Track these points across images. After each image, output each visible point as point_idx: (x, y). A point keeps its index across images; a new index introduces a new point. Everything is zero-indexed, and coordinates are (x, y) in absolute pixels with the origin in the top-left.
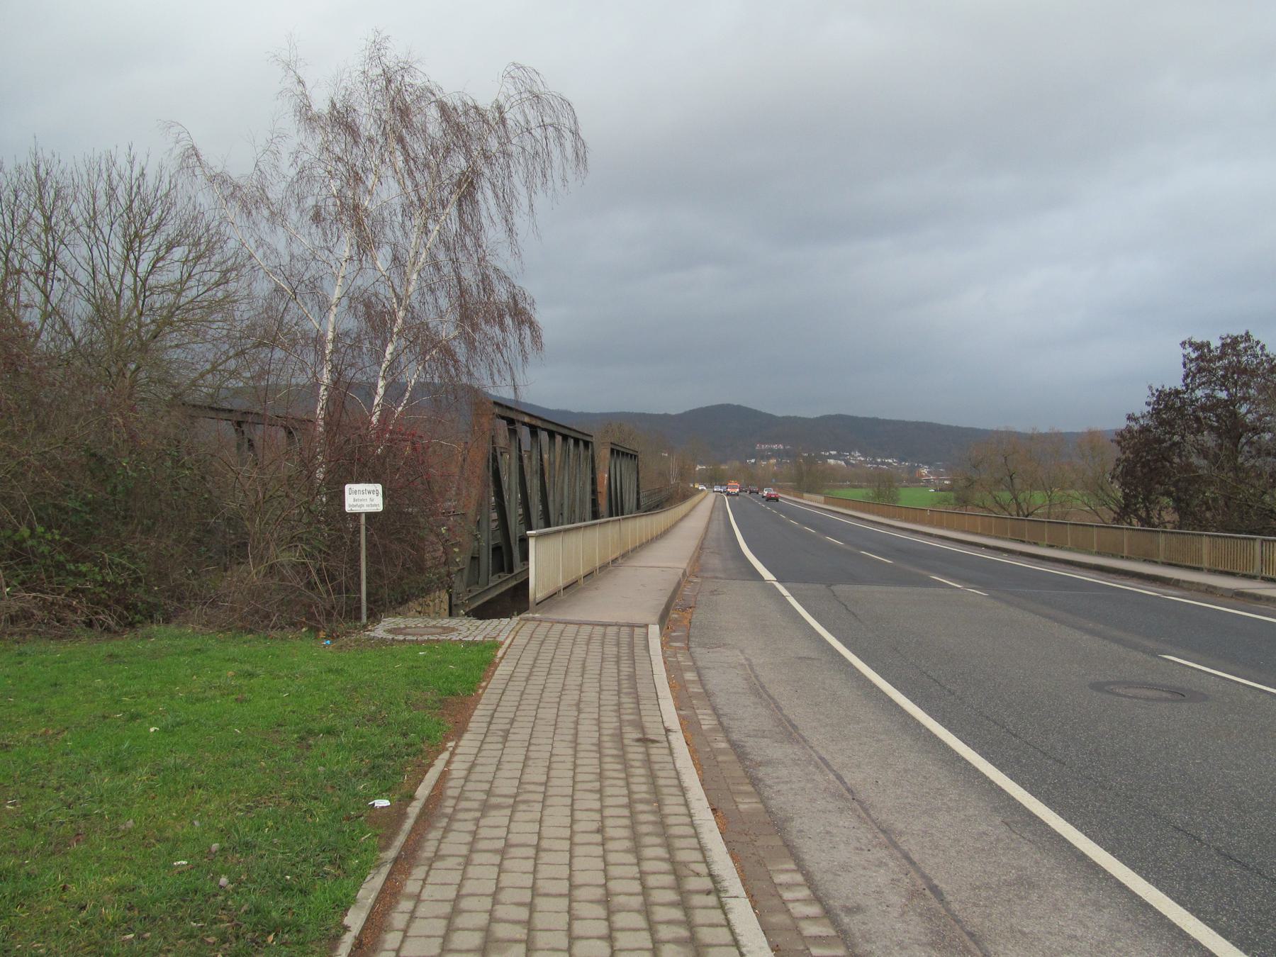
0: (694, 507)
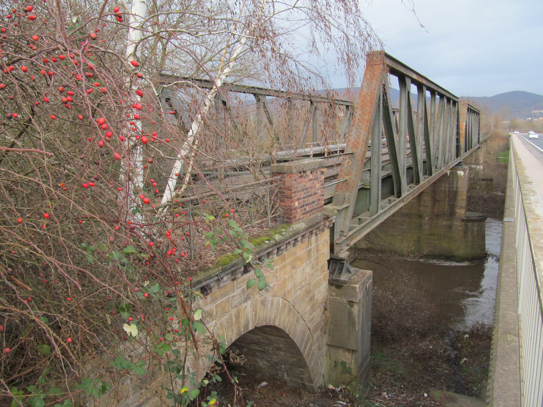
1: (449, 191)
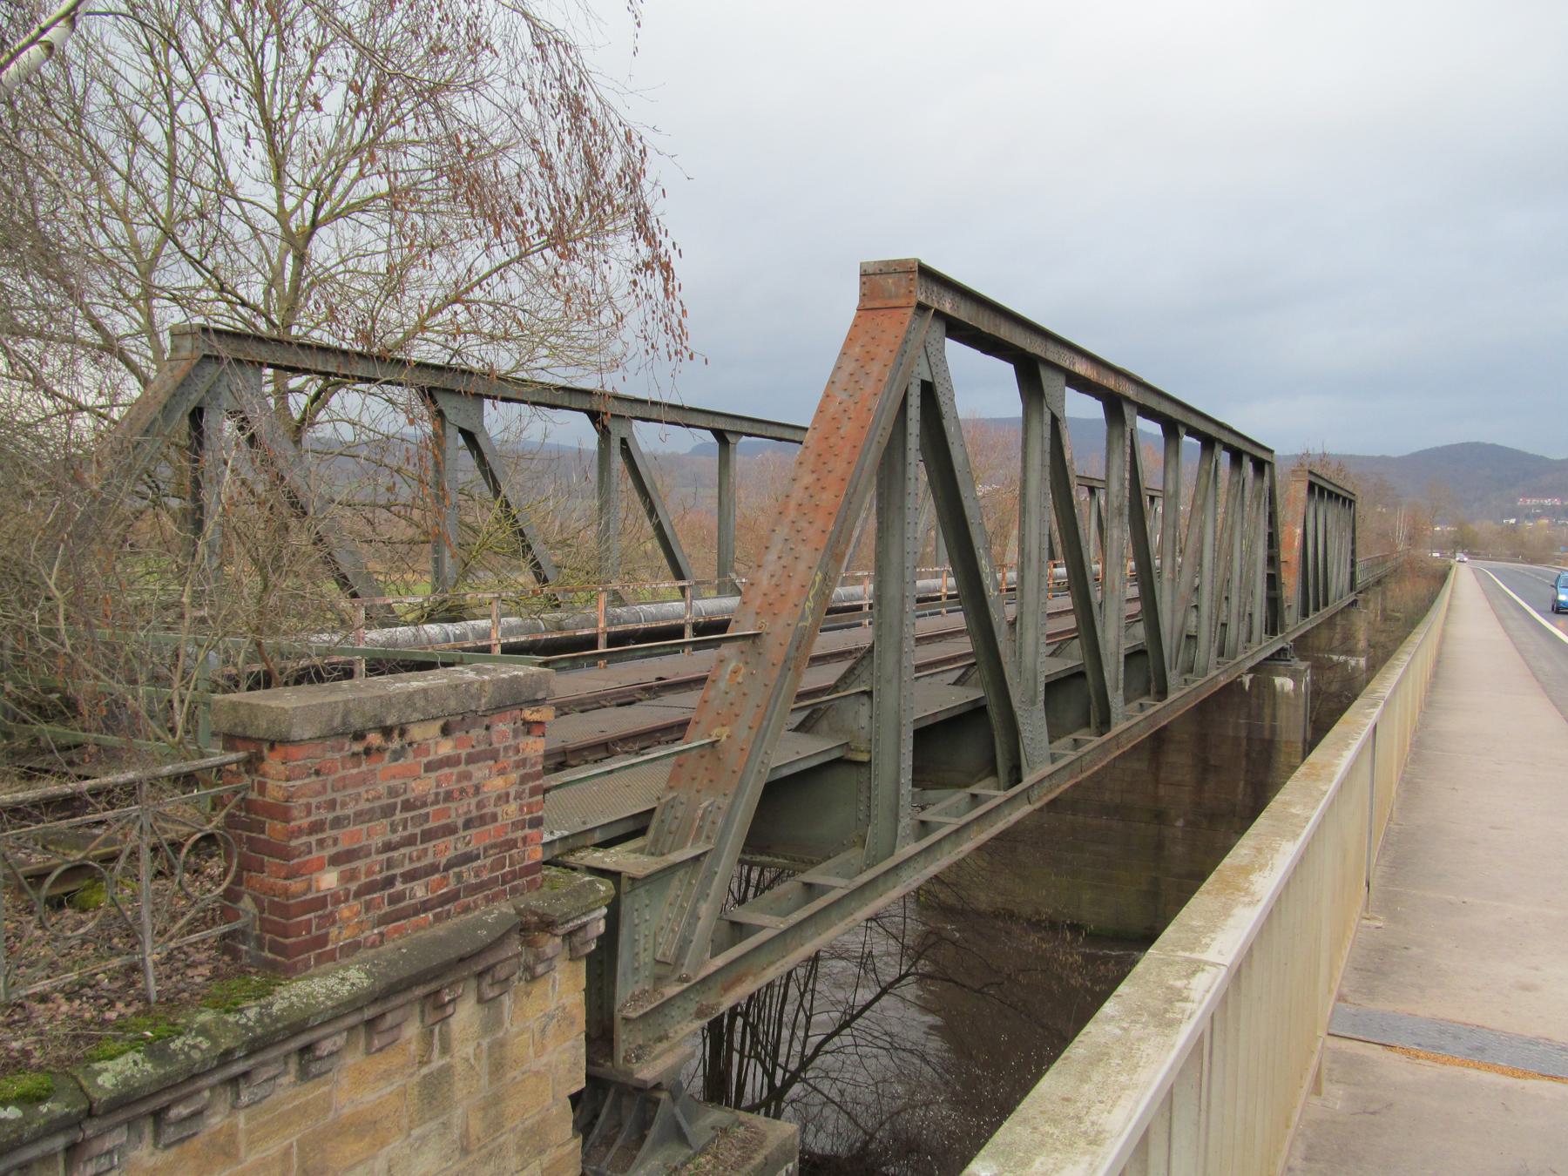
0: (1453, 591)
1: (1249, 739)
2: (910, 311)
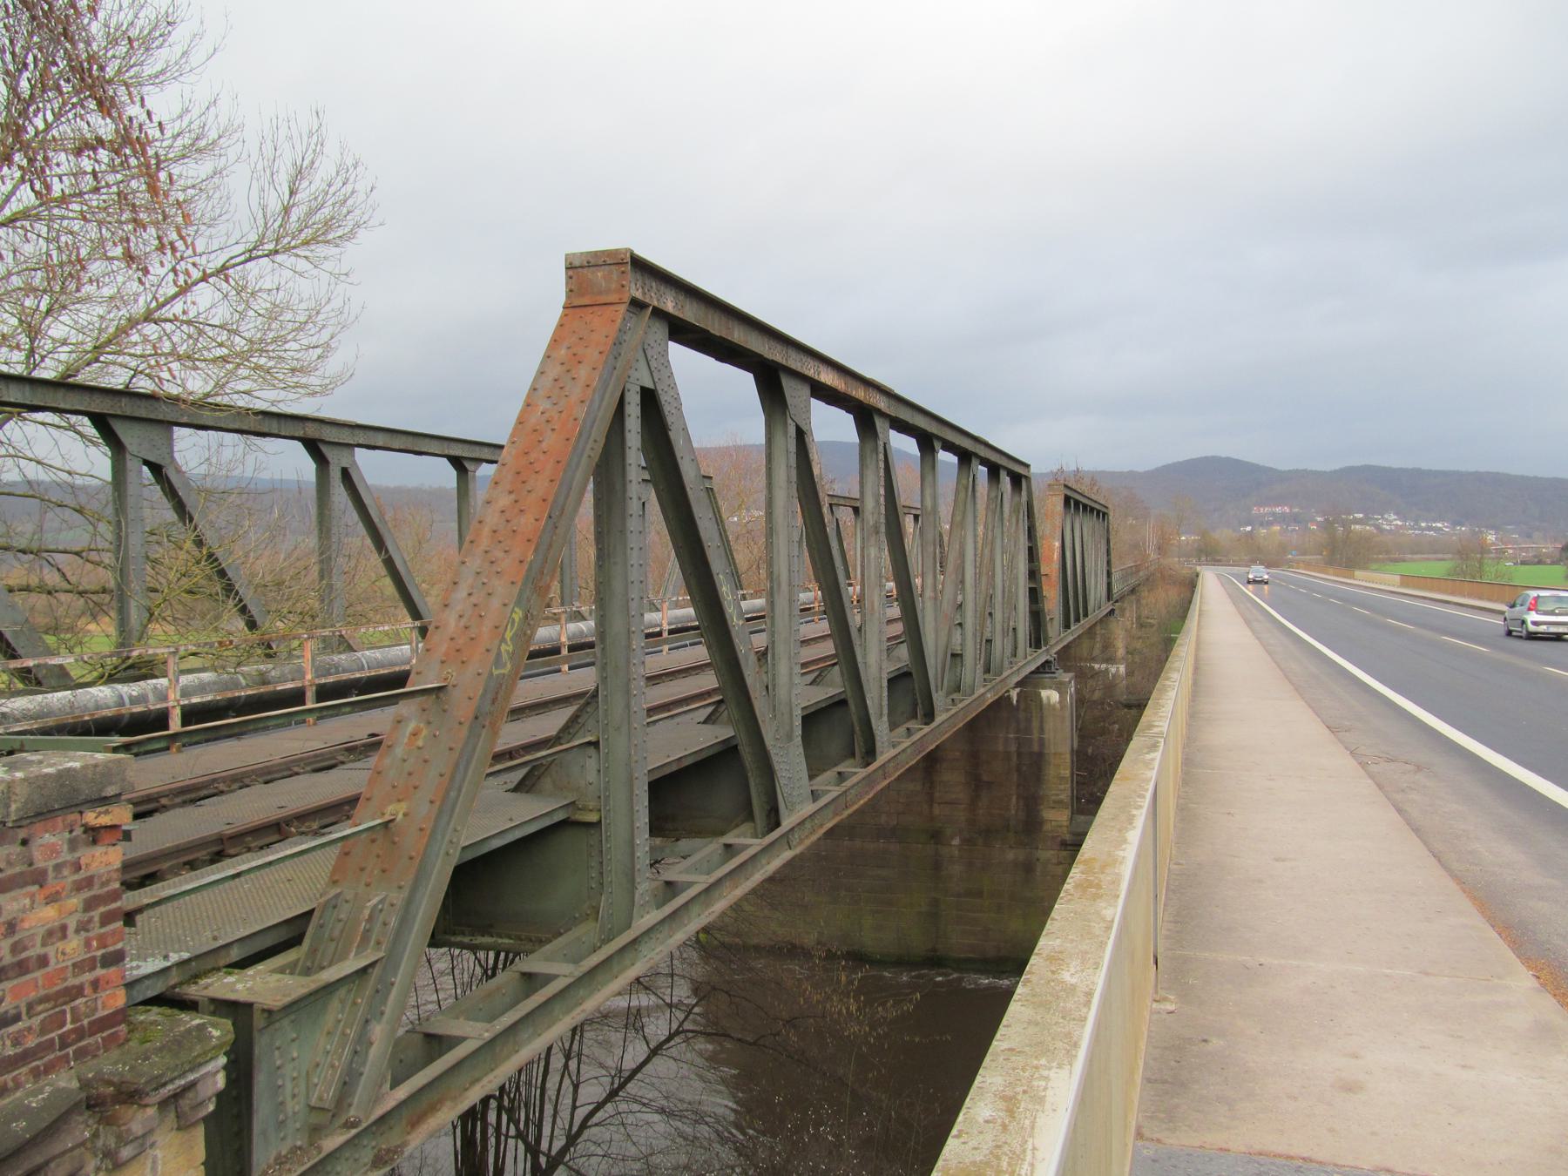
1: (1019, 754)
2: (623, 308)
